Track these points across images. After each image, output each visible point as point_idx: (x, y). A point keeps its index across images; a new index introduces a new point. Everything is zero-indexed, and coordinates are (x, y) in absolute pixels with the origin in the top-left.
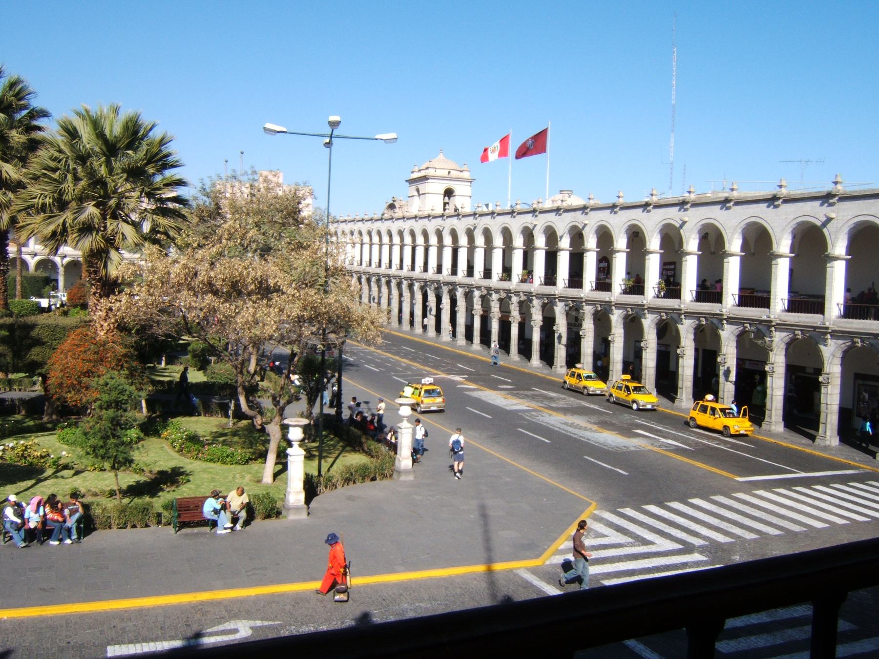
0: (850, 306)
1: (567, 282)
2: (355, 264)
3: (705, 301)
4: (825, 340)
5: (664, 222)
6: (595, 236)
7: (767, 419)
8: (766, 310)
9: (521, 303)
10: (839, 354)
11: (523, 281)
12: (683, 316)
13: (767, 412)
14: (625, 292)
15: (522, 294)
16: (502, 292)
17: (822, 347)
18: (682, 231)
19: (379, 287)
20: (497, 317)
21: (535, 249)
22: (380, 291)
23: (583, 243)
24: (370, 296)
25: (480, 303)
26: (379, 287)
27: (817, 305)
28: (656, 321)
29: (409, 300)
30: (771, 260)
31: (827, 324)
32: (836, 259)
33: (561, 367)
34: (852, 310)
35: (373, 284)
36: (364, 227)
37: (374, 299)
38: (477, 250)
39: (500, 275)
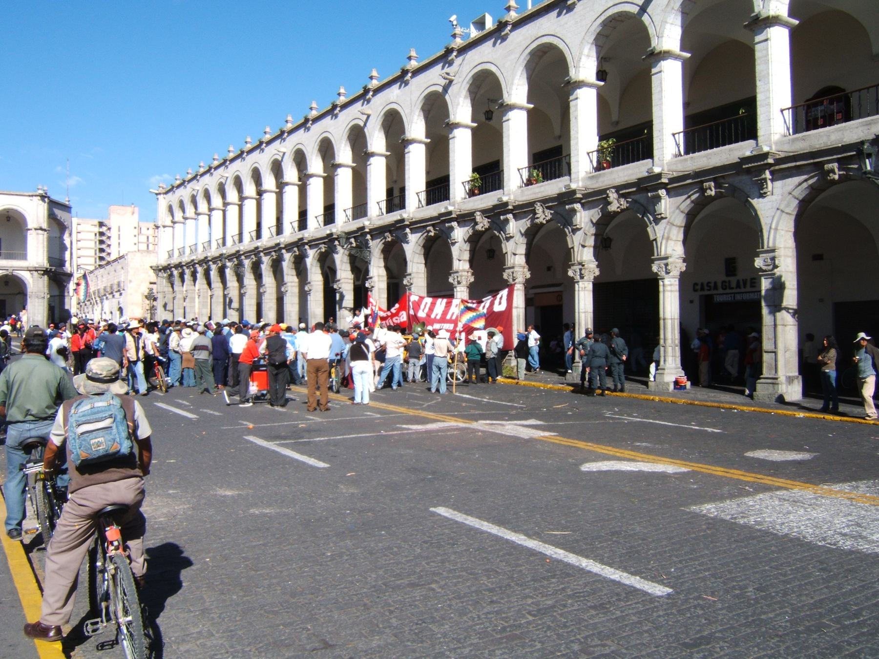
0: (693, 132)
1: (681, 138)
2: (214, 245)
3: (435, 202)
4: (761, 184)
5: (479, 68)
6: (422, 114)
7: (766, 373)
8: (650, 160)
9: (474, 240)
10: (793, 206)
11: (390, 209)
12: (408, 230)
13: (766, 357)
14: (471, 193)
15: (613, 196)
16: (539, 209)
17: (756, 202)
18: (645, 18)
19: (240, 278)
20: (675, 272)
21: (407, 142)
22: (241, 285)
23: (402, 131)
24: (225, 296)
25: (467, 256)
26: (240, 278)
27: (739, 119)
28: (422, 242)
29: (296, 290)
30: (405, 147)
31: (766, 149)
32: (580, 84)
33: (790, 380)
34: (810, 111)
35: (229, 273)
36: (210, 182)
37: (231, 301)
38: (373, 160)
39: (525, 175)
